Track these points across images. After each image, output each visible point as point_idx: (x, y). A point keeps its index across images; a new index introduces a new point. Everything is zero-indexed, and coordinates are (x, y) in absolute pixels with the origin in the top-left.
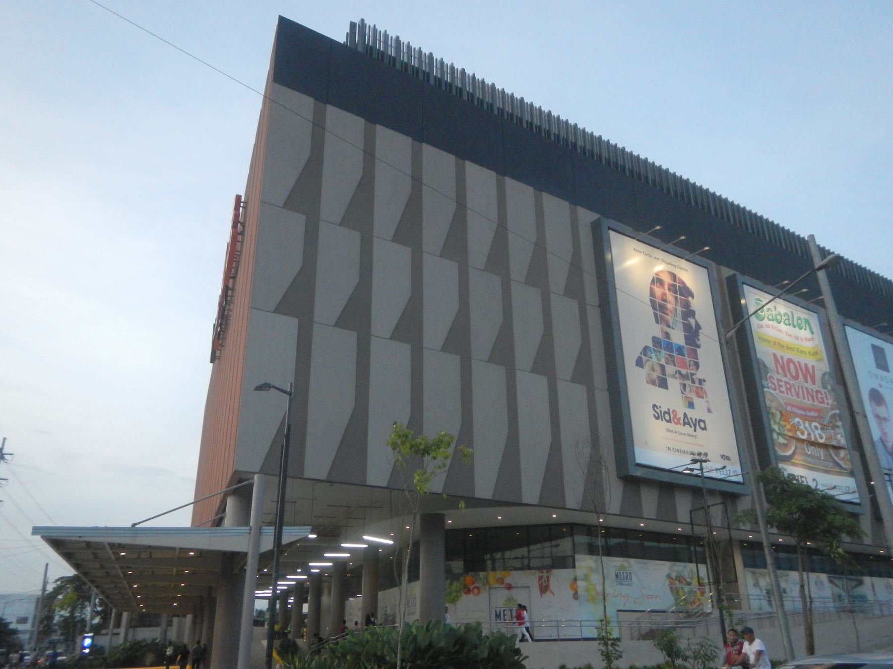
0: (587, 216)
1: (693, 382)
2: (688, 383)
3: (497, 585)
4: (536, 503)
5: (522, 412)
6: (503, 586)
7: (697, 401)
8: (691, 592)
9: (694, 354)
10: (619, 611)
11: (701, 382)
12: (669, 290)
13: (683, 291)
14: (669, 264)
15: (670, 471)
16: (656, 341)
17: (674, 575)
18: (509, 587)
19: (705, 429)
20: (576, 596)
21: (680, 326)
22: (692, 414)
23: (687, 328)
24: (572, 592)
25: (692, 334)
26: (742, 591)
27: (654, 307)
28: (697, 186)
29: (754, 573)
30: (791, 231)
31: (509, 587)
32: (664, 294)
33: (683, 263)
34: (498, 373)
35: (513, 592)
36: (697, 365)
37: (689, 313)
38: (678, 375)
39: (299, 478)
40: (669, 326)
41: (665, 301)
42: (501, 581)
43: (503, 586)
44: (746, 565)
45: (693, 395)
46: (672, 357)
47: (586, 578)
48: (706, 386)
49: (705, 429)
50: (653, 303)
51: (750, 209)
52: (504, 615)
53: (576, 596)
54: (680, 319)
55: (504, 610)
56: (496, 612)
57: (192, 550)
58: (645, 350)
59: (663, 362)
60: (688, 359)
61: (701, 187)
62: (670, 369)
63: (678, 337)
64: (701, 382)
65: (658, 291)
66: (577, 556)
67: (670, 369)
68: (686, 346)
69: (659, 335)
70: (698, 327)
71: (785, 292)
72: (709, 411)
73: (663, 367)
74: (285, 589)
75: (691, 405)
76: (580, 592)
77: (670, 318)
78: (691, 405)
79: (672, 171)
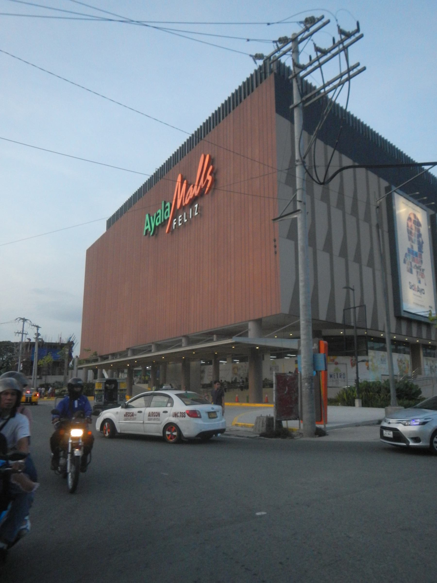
0: (384, 184)
1: (420, 270)
2: (419, 270)
3: (331, 363)
4: (382, 331)
5: (364, 285)
6: (334, 363)
7: (422, 280)
8: (405, 367)
9: (421, 256)
10: (382, 375)
11: (423, 270)
12: (414, 223)
13: (418, 224)
14: (414, 209)
15: (414, 314)
16: (409, 250)
17: (399, 359)
18: (337, 364)
19: (424, 293)
20: (368, 368)
21: (416, 242)
22: (421, 286)
23: (419, 242)
24: (366, 367)
25: (420, 245)
26: (422, 367)
27: (408, 233)
28: (286, 66)
29: (427, 359)
30: (358, 118)
31: (337, 364)
32: (411, 226)
33: (418, 209)
34: (356, 266)
35: (339, 366)
36: (422, 262)
37: (419, 235)
38: (415, 267)
39: (399, 334)
40: (413, 242)
41: (412, 229)
42: (333, 360)
43: (334, 363)
44: (424, 356)
45: (420, 277)
46: (414, 258)
47: (372, 360)
48: (425, 273)
49: (424, 293)
50: (408, 230)
51: (307, 79)
52: (334, 376)
53: (368, 368)
54: (416, 239)
55: (334, 374)
56: (330, 374)
57: (257, 346)
58: (406, 254)
59: (411, 261)
60: (419, 259)
61: (366, 125)
62: (413, 264)
63: (416, 249)
64: (423, 270)
65: (410, 224)
66: (369, 351)
67: (413, 264)
68: (419, 252)
69: (410, 247)
70: (423, 243)
71: (398, 188)
72: (426, 285)
73: (411, 263)
74: (234, 360)
75: (420, 282)
76: (370, 367)
77: (413, 238)
78: (420, 282)
79: (371, 128)
